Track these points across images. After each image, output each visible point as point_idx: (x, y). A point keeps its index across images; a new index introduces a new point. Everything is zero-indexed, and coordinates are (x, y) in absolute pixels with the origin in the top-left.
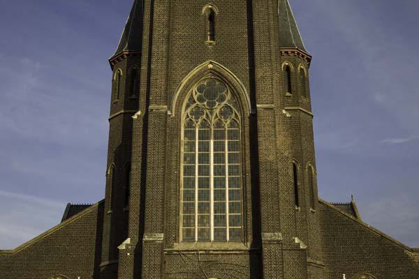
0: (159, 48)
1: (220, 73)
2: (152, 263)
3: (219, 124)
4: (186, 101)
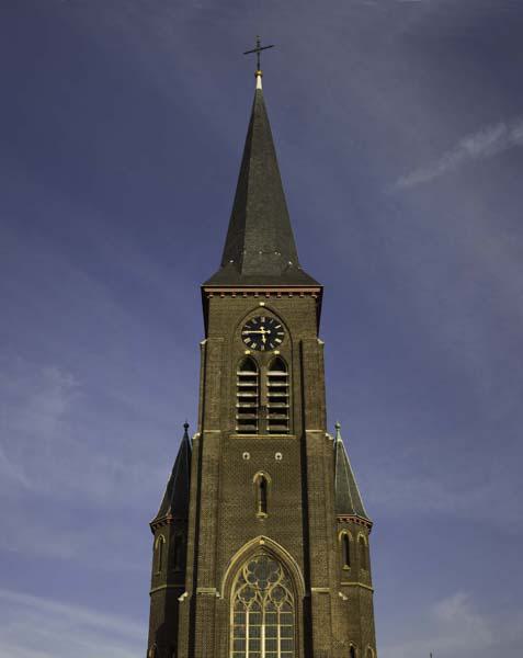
0: (207, 523)
3: (271, 607)
4: (236, 580)
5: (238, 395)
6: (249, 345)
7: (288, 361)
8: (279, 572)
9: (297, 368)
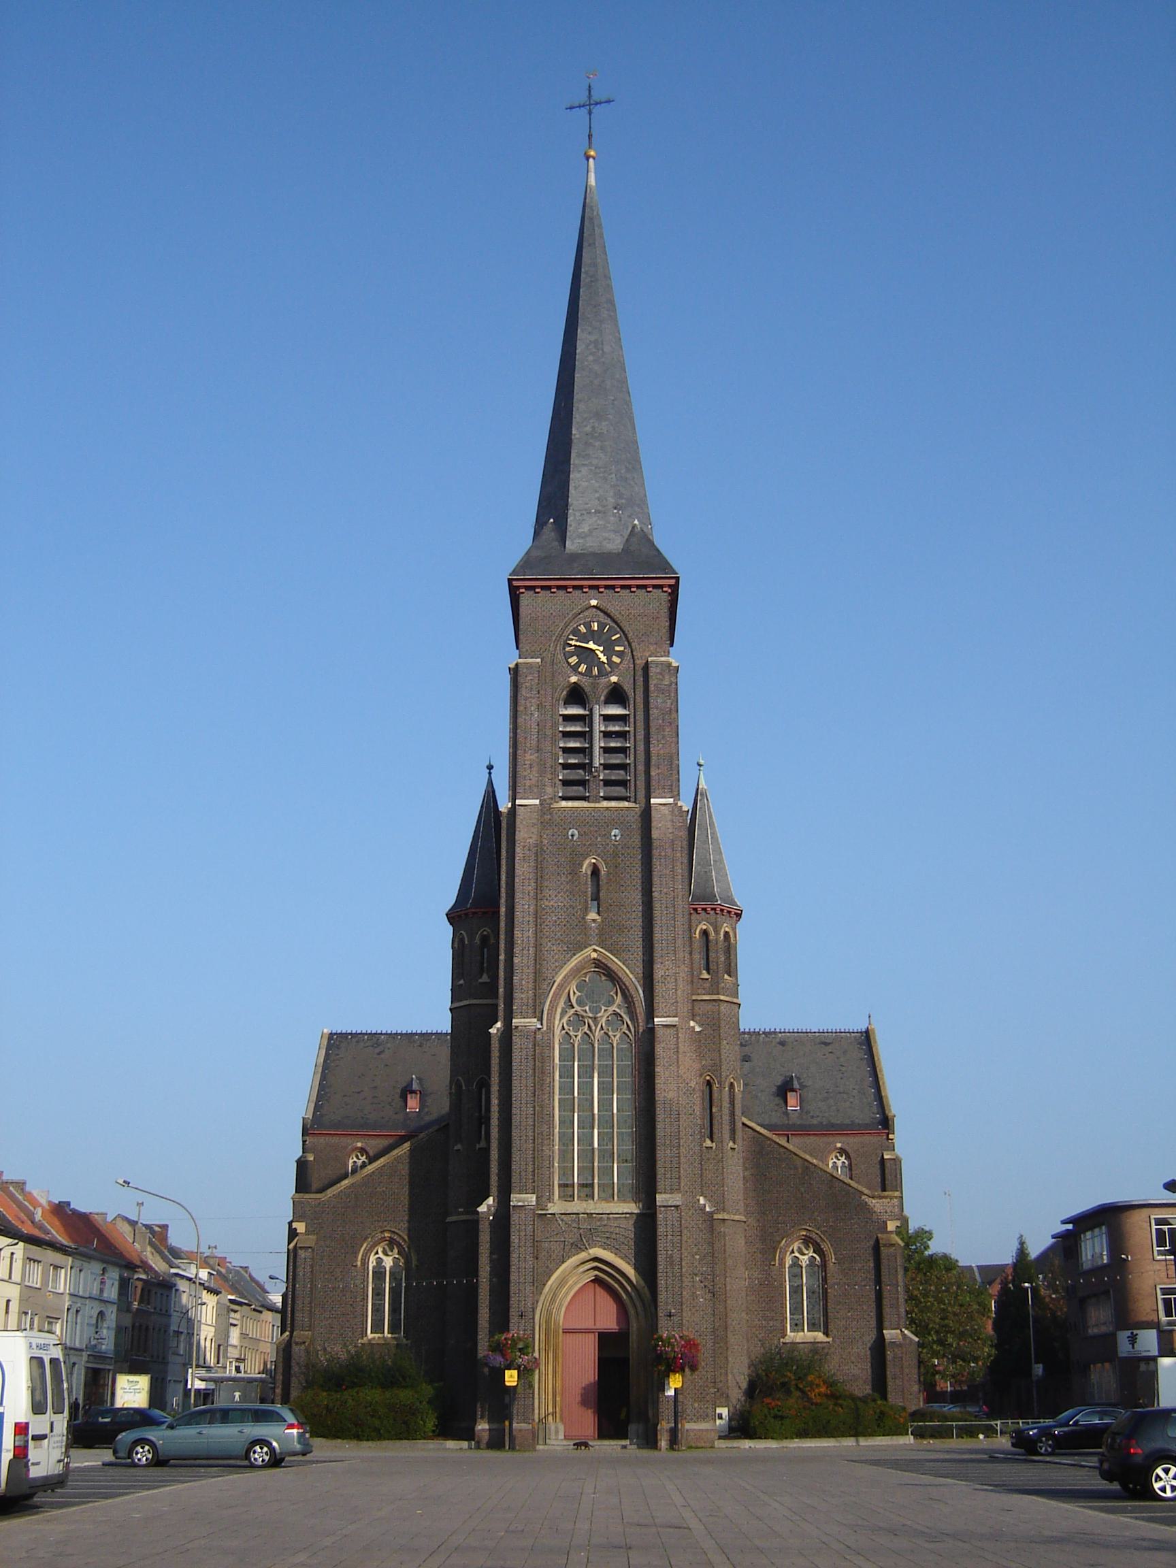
1: (607, 966)
4: (562, 1004)
5: (562, 745)
6: (575, 668)
7: (630, 693)
9: (640, 706)
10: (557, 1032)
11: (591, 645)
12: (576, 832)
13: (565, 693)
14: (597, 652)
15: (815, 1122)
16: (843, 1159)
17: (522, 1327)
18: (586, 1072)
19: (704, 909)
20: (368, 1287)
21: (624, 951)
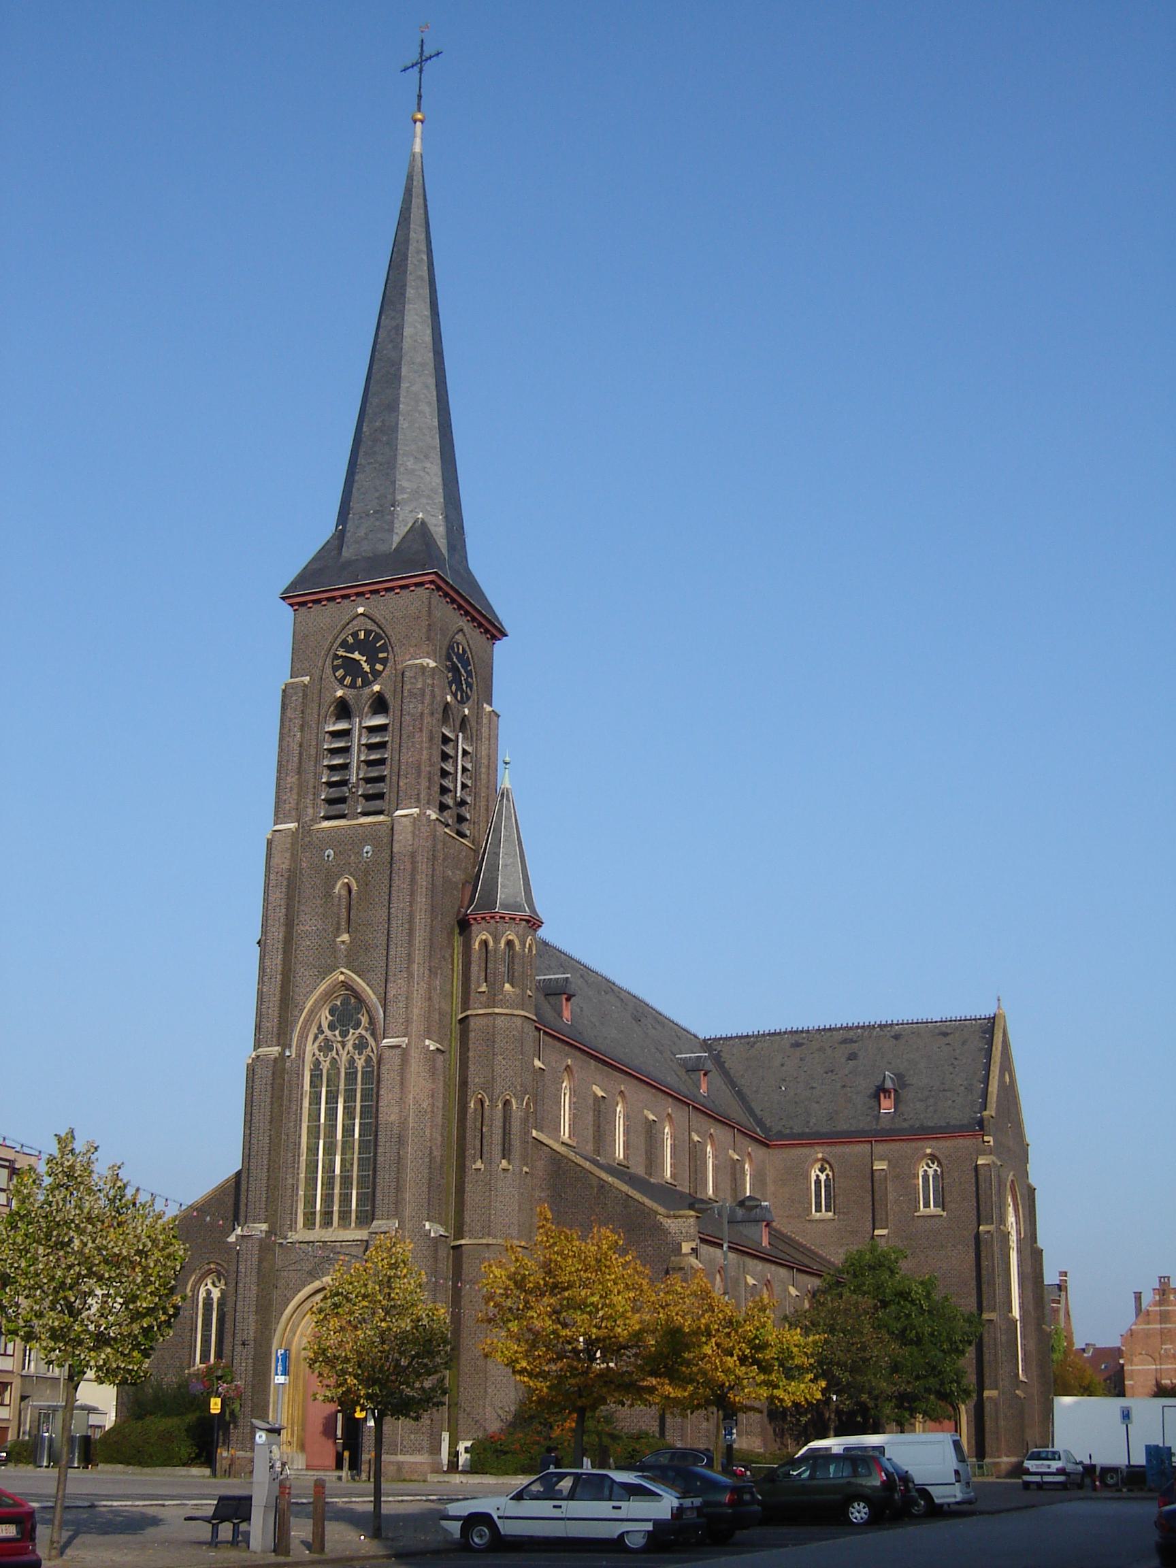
2: (249, 1263)
4: (314, 1030)
8: (363, 1015)
10: (308, 1058)
11: (356, 656)
12: (332, 852)
13: (332, 708)
14: (362, 662)
15: (905, 1125)
16: (935, 1167)
17: (244, 1354)
18: (332, 1099)
19: (483, 918)
20: (197, 1318)
21: (369, 971)
